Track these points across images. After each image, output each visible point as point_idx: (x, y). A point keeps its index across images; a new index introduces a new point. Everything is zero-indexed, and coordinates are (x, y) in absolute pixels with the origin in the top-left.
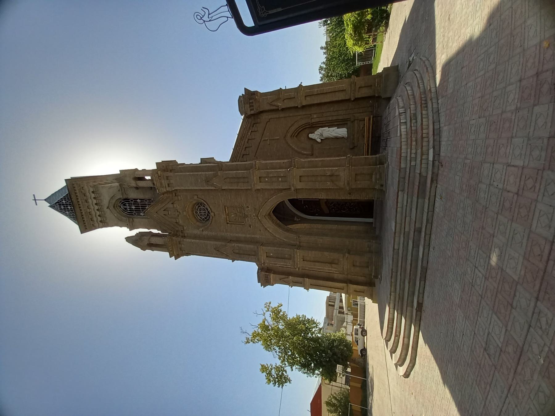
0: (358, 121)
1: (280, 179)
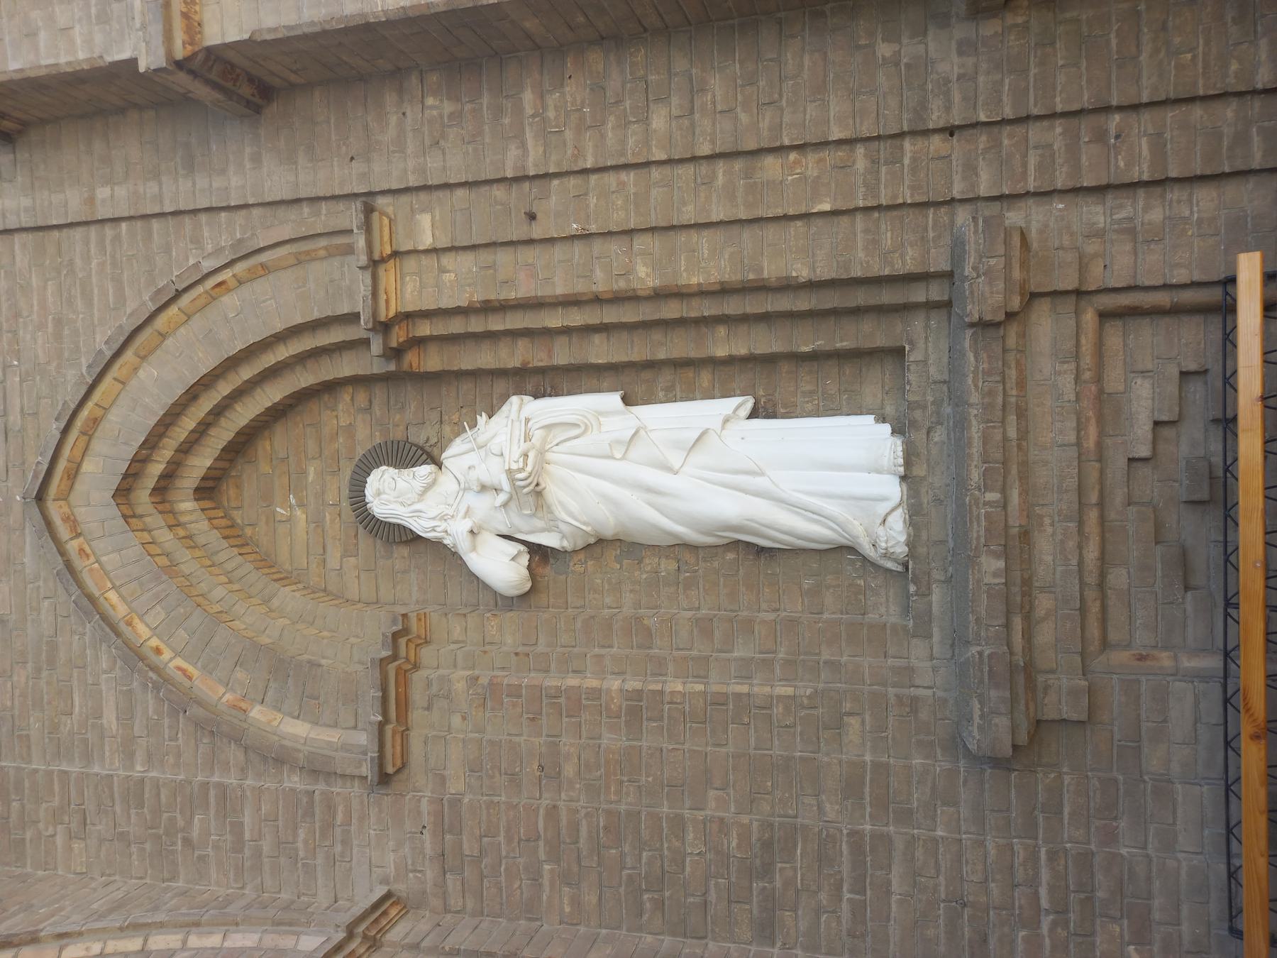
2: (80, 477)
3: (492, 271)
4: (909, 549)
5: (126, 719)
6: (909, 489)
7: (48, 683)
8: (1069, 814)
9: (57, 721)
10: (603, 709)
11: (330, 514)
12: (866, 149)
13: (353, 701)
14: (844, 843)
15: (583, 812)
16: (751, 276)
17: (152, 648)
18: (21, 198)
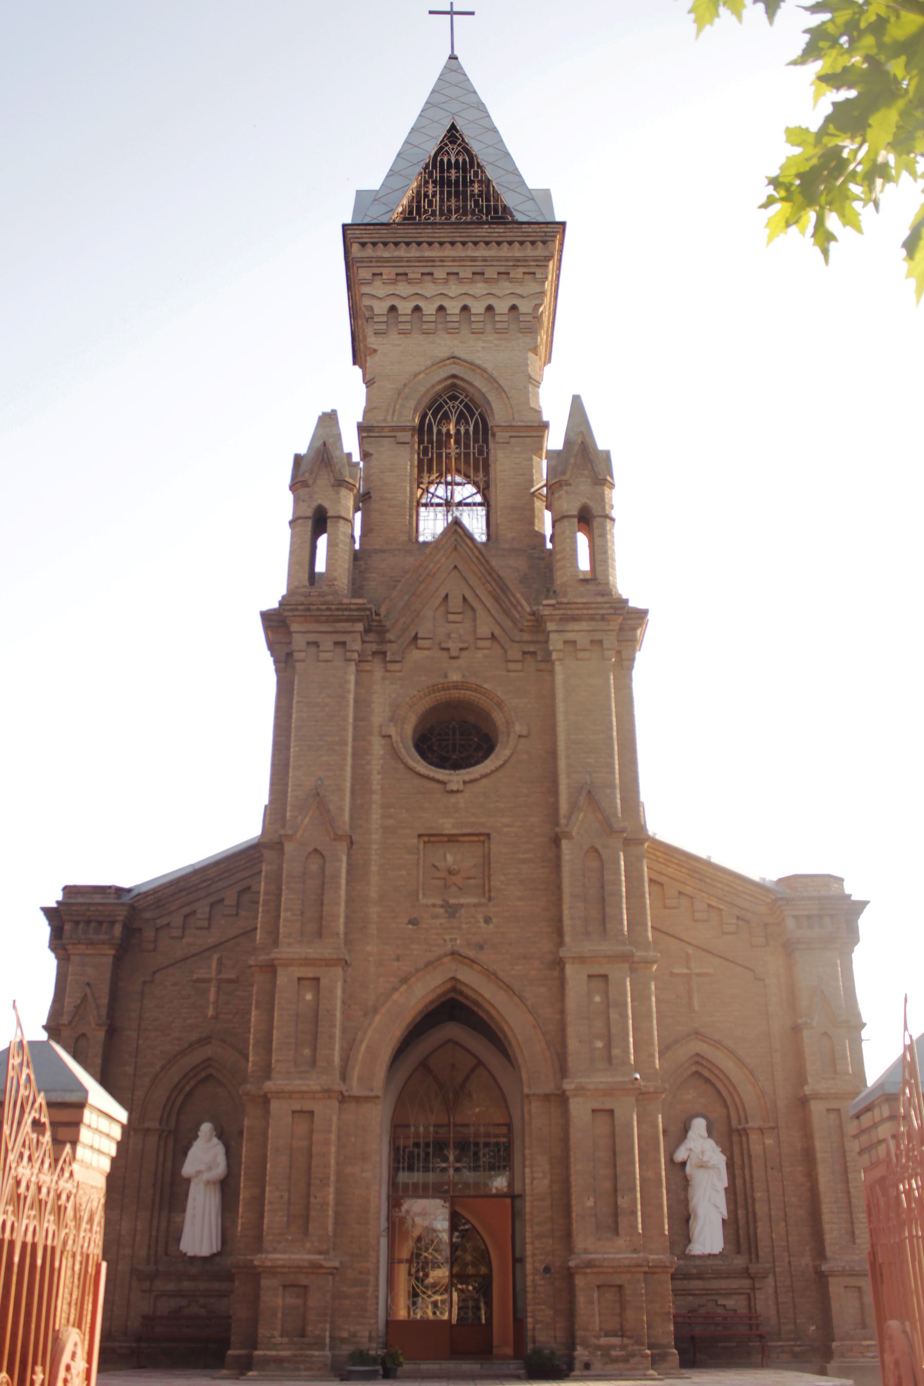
0: (748, 1291)
1: (599, 1044)
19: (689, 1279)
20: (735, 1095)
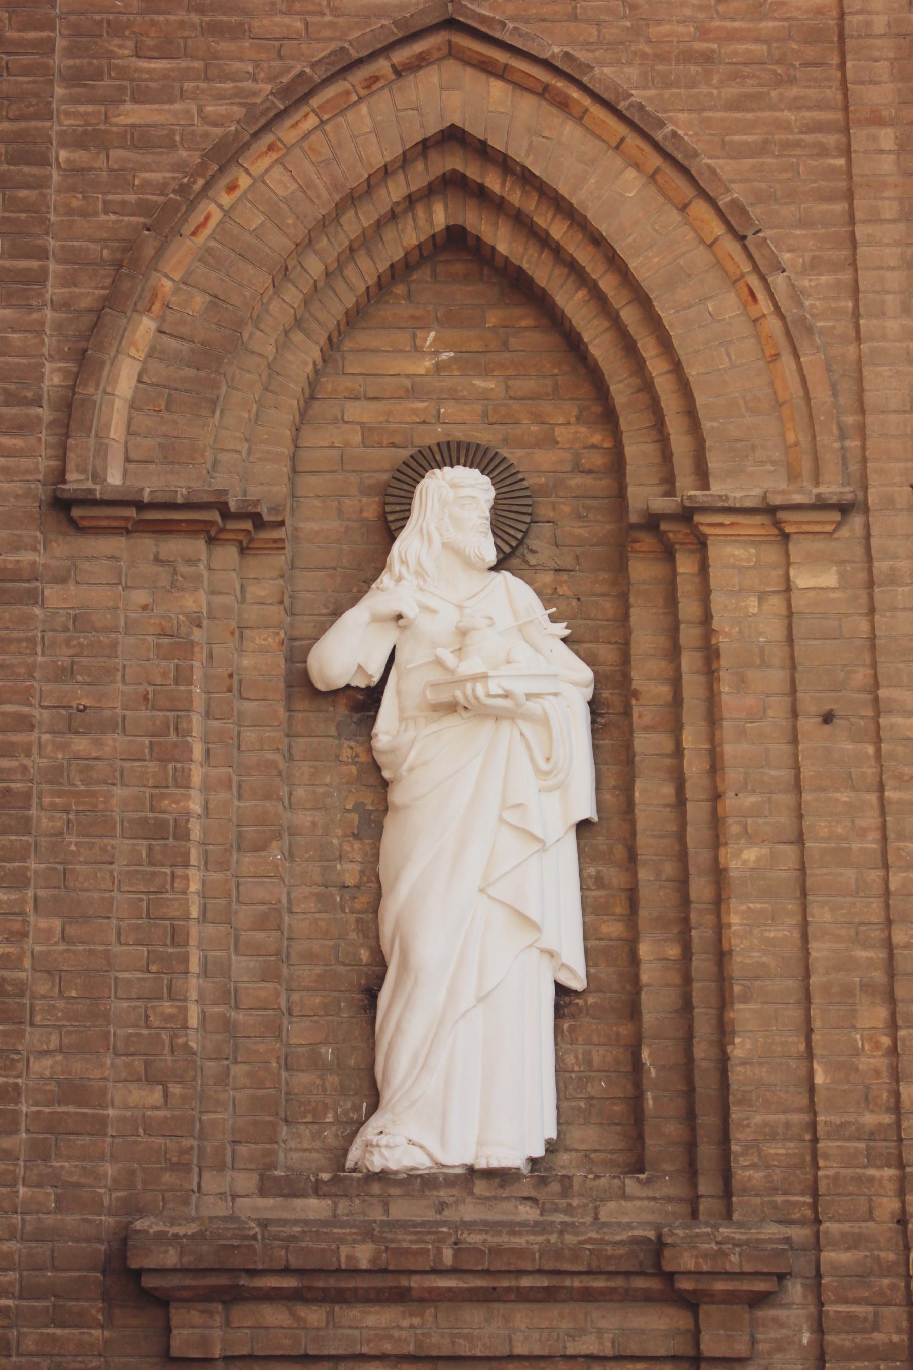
2: (482, 77)
3: (758, 662)
4: (377, 1174)
5: (132, 138)
6: (457, 1176)
7: (182, 24)
8: (54, 1334)
9: (127, 33)
10: (164, 790)
11: (426, 408)
12: (888, 1125)
13: (165, 457)
14: (4, 1079)
15: (27, 762)
16: (737, 989)
17: (237, 179)
18: (885, 18)
19: (341, 1297)
20: (648, 348)
